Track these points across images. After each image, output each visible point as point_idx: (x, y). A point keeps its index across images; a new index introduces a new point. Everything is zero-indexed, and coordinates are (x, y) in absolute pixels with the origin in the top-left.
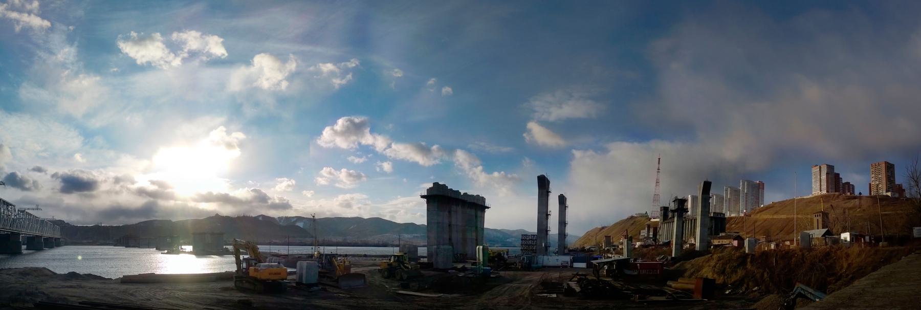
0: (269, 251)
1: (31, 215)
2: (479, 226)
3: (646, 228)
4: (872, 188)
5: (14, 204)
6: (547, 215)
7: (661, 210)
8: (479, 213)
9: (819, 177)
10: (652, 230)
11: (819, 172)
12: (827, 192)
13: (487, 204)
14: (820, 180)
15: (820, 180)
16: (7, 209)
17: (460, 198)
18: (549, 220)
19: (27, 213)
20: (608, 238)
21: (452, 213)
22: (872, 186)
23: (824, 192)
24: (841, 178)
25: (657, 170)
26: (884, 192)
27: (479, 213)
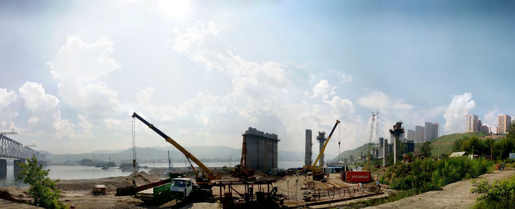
0: (166, 166)
1: (30, 149)
2: (274, 151)
3: (372, 150)
4: (498, 129)
5: (22, 144)
6: (311, 144)
7: (380, 140)
8: (274, 144)
9: (469, 122)
10: (375, 151)
11: (469, 119)
12: (474, 130)
13: (278, 139)
14: (470, 124)
15: (470, 124)
16: (19, 146)
17: (264, 136)
18: (312, 147)
19: (29, 148)
20: (351, 157)
21: (259, 144)
22: (498, 128)
23: (472, 131)
24: (482, 123)
25: (377, 118)
26: (505, 132)
27: (274, 144)
